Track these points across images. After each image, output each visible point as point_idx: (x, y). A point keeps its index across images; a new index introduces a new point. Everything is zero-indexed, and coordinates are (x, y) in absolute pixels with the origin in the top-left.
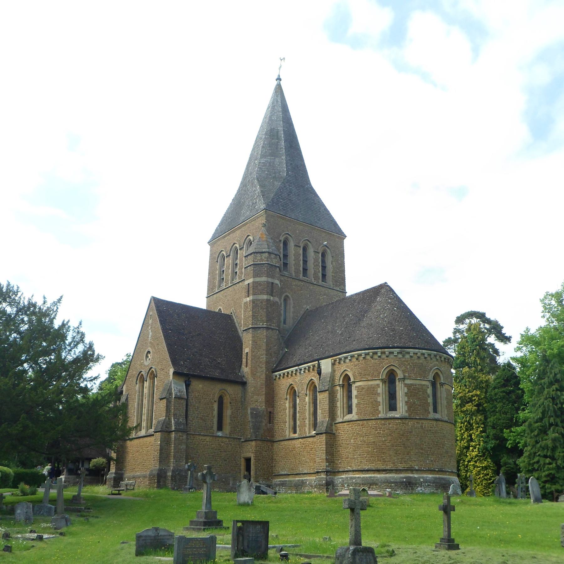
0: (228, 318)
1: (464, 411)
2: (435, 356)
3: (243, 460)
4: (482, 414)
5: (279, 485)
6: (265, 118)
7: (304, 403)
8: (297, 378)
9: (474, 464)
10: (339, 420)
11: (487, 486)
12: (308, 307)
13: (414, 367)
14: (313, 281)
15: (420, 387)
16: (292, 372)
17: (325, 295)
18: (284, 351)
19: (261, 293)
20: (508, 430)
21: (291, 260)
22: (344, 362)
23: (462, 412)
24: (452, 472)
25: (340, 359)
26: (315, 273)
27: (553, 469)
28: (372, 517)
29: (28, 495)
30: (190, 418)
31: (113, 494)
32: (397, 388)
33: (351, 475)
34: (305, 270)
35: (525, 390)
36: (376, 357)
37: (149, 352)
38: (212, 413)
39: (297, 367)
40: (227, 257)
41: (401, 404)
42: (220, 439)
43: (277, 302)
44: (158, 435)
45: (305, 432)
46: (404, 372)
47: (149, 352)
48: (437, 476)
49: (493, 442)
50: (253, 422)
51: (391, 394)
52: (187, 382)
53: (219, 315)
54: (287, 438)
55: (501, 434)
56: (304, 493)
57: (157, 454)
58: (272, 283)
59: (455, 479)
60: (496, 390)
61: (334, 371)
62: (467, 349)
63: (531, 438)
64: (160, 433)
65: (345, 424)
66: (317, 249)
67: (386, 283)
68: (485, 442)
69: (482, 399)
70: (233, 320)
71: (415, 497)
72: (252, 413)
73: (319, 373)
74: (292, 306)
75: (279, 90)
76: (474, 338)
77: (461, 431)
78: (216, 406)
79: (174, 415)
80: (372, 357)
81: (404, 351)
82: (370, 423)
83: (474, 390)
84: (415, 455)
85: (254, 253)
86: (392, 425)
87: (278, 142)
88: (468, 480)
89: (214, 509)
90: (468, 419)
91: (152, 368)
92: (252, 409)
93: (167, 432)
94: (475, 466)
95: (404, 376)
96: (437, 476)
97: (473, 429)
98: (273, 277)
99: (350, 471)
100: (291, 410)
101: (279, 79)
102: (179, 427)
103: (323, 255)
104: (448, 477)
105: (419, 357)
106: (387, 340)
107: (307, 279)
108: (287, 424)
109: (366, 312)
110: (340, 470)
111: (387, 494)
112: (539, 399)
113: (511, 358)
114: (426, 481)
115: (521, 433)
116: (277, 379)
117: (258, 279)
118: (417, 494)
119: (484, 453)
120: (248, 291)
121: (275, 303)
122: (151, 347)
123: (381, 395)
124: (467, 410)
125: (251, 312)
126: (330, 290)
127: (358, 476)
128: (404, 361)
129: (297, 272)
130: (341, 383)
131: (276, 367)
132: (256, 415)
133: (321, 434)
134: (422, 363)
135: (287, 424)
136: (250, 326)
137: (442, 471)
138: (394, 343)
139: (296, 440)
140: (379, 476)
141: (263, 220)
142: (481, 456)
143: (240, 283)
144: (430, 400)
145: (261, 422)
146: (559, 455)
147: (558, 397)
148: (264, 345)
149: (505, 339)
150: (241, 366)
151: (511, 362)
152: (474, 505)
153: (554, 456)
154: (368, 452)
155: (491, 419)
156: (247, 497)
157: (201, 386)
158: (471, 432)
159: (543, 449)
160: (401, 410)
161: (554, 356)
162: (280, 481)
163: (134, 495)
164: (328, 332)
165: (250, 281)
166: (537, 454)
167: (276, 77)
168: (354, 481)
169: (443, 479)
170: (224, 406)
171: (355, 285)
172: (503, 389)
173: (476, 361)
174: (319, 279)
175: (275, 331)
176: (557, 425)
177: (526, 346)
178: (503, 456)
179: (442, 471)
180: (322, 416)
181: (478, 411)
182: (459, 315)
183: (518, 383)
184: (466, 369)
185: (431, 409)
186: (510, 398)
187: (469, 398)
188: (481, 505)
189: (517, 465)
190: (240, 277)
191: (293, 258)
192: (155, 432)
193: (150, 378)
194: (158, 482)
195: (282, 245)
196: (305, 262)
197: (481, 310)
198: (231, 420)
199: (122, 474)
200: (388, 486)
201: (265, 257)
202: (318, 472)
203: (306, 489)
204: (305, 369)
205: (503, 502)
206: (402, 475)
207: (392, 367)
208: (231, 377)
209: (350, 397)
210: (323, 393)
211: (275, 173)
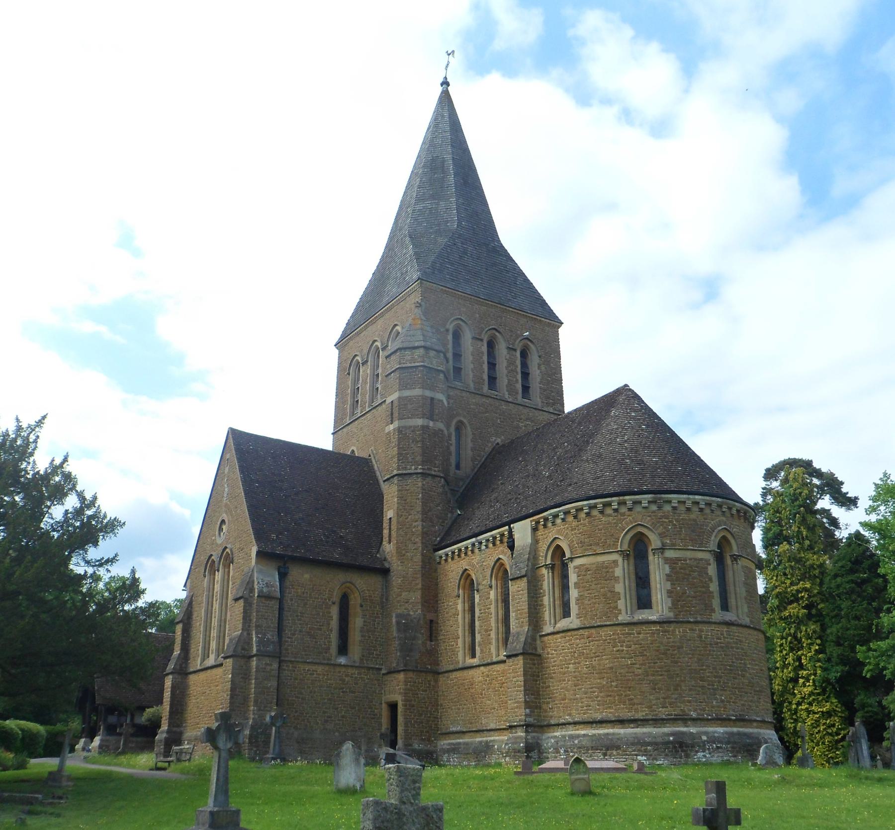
1: (786, 618)
2: (720, 506)
3: (384, 706)
4: (816, 622)
5: (448, 751)
6: (424, 143)
7: (487, 602)
8: (475, 558)
9: (807, 709)
10: (548, 629)
11: (834, 745)
12: (499, 440)
13: (681, 528)
14: (507, 396)
16: (467, 548)
17: (527, 419)
18: (455, 515)
19: (413, 416)
20: (864, 648)
22: (554, 523)
23: (781, 618)
24: (763, 722)
25: (546, 519)
26: (510, 385)
28: (590, 817)
30: (287, 632)
32: (651, 567)
33: (571, 731)
34: (492, 380)
35: (890, 577)
36: (609, 511)
37: (223, 522)
39: (474, 540)
40: (363, 364)
41: (659, 597)
42: (343, 669)
43: (442, 431)
44: (229, 661)
45: (490, 654)
46: (662, 536)
47: (223, 522)
48: (735, 730)
49: (839, 668)
51: (640, 578)
53: (352, 459)
55: (852, 655)
56: (489, 765)
58: (432, 399)
59: (771, 734)
60: (839, 580)
61: (536, 541)
62: (785, 514)
66: (513, 344)
67: (626, 385)
68: (824, 670)
69: (814, 596)
70: (373, 466)
71: (689, 771)
72: (398, 623)
73: (511, 547)
75: (446, 100)
76: (794, 494)
77: (781, 651)
78: (335, 611)
79: (257, 626)
80: (602, 512)
81: (660, 499)
82: (603, 632)
83: (800, 580)
84: (690, 690)
87: (443, 177)
88: (799, 737)
89: (233, 806)
90: (792, 631)
91: (226, 548)
92: (399, 616)
93: (243, 657)
94: (809, 712)
95: (663, 544)
96: (735, 730)
97: (802, 647)
98: (432, 388)
99: (569, 724)
100: (467, 616)
101: (445, 83)
103: (524, 354)
104: (756, 730)
105: (688, 509)
106: (629, 480)
107: (496, 393)
108: (460, 641)
109: (592, 435)
110: (553, 722)
111: (635, 766)
113: (860, 523)
114: (713, 740)
115: (887, 651)
116: (443, 562)
117: (407, 393)
118: (696, 765)
119: (825, 688)
120: (392, 414)
121: (437, 433)
123: (621, 580)
124: (790, 615)
126: (536, 412)
127: (583, 732)
128: (662, 517)
130: (549, 562)
132: (406, 626)
133: (516, 655)
134: (695, 520)
135: (460, 641)
136: (395, 472)
137: (743, 720)
138: (642, 485)
139: (475, 670)
140: (622, 731)
141: (416, 297)
142: (819, 694)
144: (714, 587)
145: (415, 638)
149: (849, 502)
150: (381, 543)
151: (862, 532)
152: (808, 785)
154: (601, 688)
155: (833, 630)
156: (353, 775)
157: (307, 576)
158: (799, 653)
160: (660, 607)
162: (449, 744)
164: (528, 476)
165: (394, 396)
167: (441, 80)
168: (576, 742)
169: (745, 734)
170: (351, 611)
172: (850, 578)
173: (801, 533)
174: (517, 393)
177: (885, 502)
178: (859, 694)
179: (743, 720)
180: (519, 624)
181: (809, 616)
182: (769, 466)
183: (876, 565)
184: (785, 546)
185: (716, 603)
186: (864, 591)
187: (793, 595)
188: (821, 786)
189: (884, 708)
191: (471, 358)
193: (224, 566)
197: (805, 456)
199: (181, 733)
200: (639, 750)
202: (511, 727)
203: (493, 759)
204: (488, 541)
205: (867, 778)
208: (364, 561)
209: (565, 588)
210: (518, 582)
211: (439, 225)
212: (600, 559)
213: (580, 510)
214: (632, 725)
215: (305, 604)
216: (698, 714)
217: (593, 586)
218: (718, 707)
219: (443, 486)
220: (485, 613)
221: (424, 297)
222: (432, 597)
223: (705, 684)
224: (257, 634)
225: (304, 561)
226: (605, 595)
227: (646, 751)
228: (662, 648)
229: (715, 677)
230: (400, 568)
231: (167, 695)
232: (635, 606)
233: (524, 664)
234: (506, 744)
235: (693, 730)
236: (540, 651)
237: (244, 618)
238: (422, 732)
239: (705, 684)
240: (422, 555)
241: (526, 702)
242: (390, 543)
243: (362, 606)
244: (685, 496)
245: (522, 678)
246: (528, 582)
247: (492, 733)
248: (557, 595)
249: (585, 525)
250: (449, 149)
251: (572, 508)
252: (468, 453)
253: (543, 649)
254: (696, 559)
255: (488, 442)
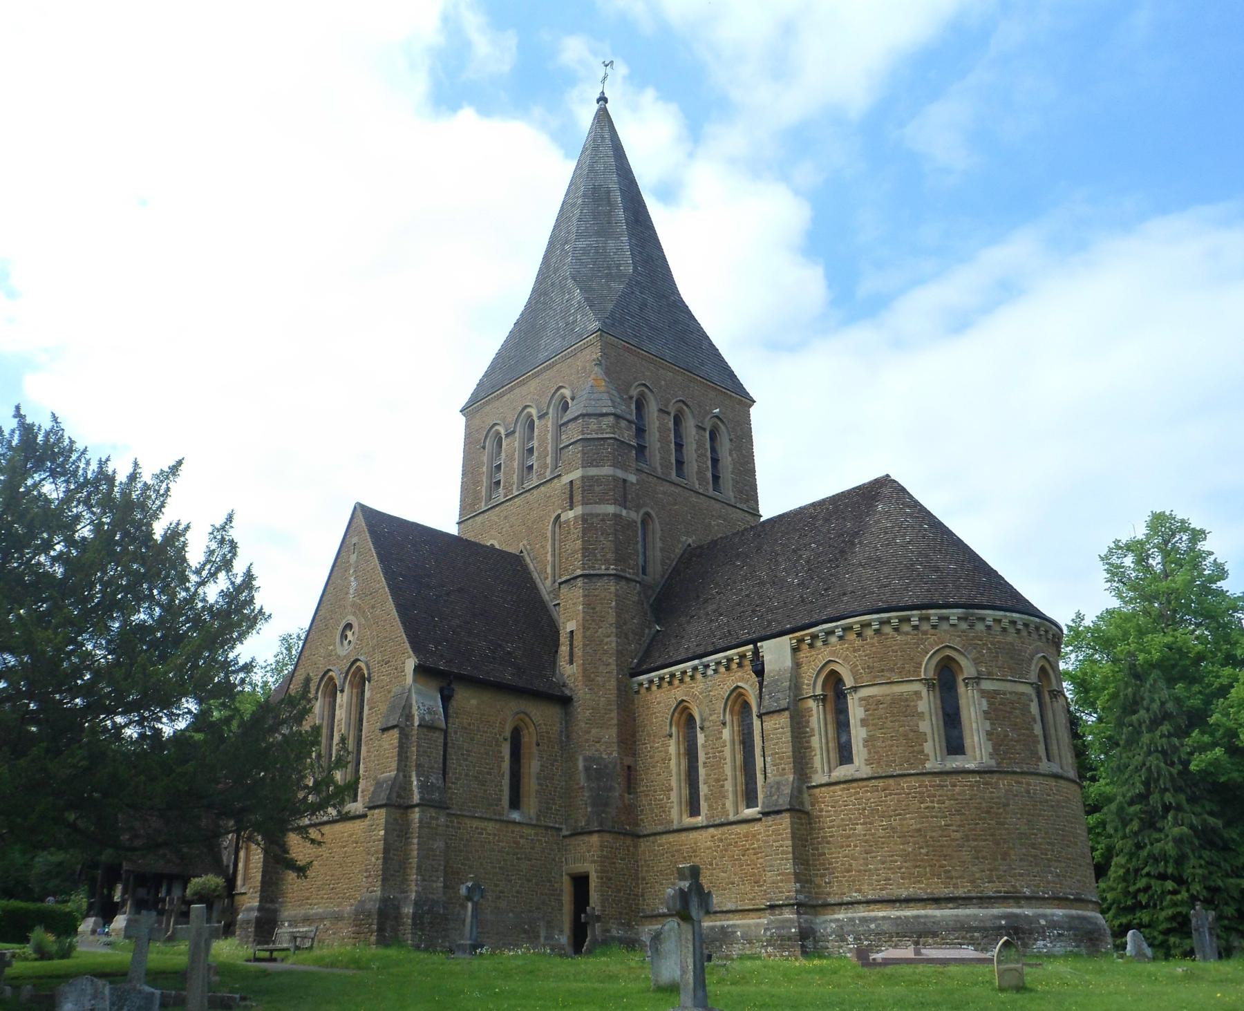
8: (706, 686)
12: (690, 541)
15: (1014, 698)
18: (653, 631)
19: (607, 502)
21: (653, 439)
22: (825, 643)
25: (814, 637)
26: (700, 472)
27: (1183, 903)
29: (50, 958)
31: (257, 960)
33: (861, 913)
34: (680, 463)
37: (349, 626)
38: (500, 767)
39: (696, 662)
41: (976, 739)
42: (517, 829)
46: (976, 662)
47: (349, 626)
48: (1074, 912)
50: (591, 790)
52: (446, 692)
54: (675, 826)
57: (376, 861)
58: (625, 481)
61: (797, 665)
63: (1124, 837)
64: (383, 811)
65: (837, 787)
67: (888, 476)
72: (587, 769)
73: (760, 672)
74: (658, 535)
75: (603, 118)
78: (506, 750)
79: (418, 766)
80: (896, 630)
81: (973, 615)
84: (1021, 860)
85: (583, 415)
86: (962, 787)
93: (399, 807)
96: (1074, 912)
98: (624, 467)
99: (859, 903)
100: (683, 761)
101: (603, 99)
102: (428, 800)
105: (1004, 630)
106: (928, 590)
108: (674, 796)
110: (831, 900)
112: (1130, 754)
114: (1053, 925)
115: (1097, 827)
116: (643, 691)
117: (593, 471)
122: (354, 614)
123: (927, 716)
125: (579, 542)
127: (881, 914)
128: (974, 638)
130: (819, 691)
131: (639, 664)
132: (597, 772)
134: (1012, 644)
135: (674, 796)
136: (579, 572)
140: (938, 913)
141: (595, 353)
143: (542, 488)
144: (1038, 729)
145: (611, 789)
146: (1194, 875)
147: (1175, 749)
148: (612, 613)
150: (554, 663)
153: (1181, 876)
157: (474, 702)
159: (1156, 860)
160: (978, 752)
161: (1153, 666)
163: (319, 961)
164: (763, 583)
165: (576, 475)
166: (1144, 872)
169: (1084, 918)
176: (1179, 808)
180: (774, 769)
185: (932, 747)
190: (540, 476)
191: (657, 435)
192: (370, 808)
194: (381, 930)
198: (540, 784)
199: (276, 911)
201: (608, 426)
202: (772, 907)
210: (775, 716)
213: (867, 625)
214: (951, 905)
215: (472, 739)
216: (1033, 892)
217: (889, 724)
218: (1054, 882)
219: (639, 593)
220: (715, 757)
221: (604, 354)
222: (630, 734)
223: (1038, 852)
224: (418, 776)
226: (905, 736)
227: (972, 938)
228: (984, 805)
229: (1049, 844)
230: (588, 696)
232: (945, 751)
233: (792, 823)
234: (766, 930)
235: (1028, 912)
236: (808, 808)
237: (400, 754)
238: (621, 913)
239: (1038, 852)
240: (618, 680)
241: (796, 874)
242: (571, 662)
243: (538, 745)
244: (1002, 613)
245: (790, 843)
246: (792, 718)
247: (731, 915)
248: (830, 735)
249: (873, 645)
250: (615, 177)
251: (856, 623)
252: (656, 554)
253: (813, 805)
254: (1016, 693)
255: (679, 541)
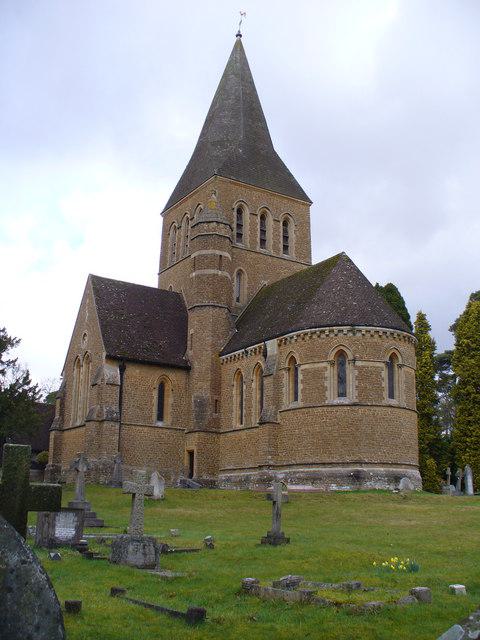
0: (178, 296)
2: (392, 334)
12: (266, 282)
21: (246, 231)
36: (323, 336)
73: (265, 356)
78: (155, 394)
98: (220, 249)
101: (239, 35)
105: (372, 336)
114: (376, 475)
121: (223, 279)
129: (253, 242)
132: (201, 404)
140: (324, 469)
144: (385, 384)
157: (138, 371)
171: (317, 258)
175: (223, 310)
185: (386, 393)
195: (235, 213)
196: (263, 232)
206: (350, 469)
207: (342, 348)
208: (172, 361)
209: (296, 382)
212: (316, 366)
222: (216, 386)
225: (136, 362)
231: (51, 443)
